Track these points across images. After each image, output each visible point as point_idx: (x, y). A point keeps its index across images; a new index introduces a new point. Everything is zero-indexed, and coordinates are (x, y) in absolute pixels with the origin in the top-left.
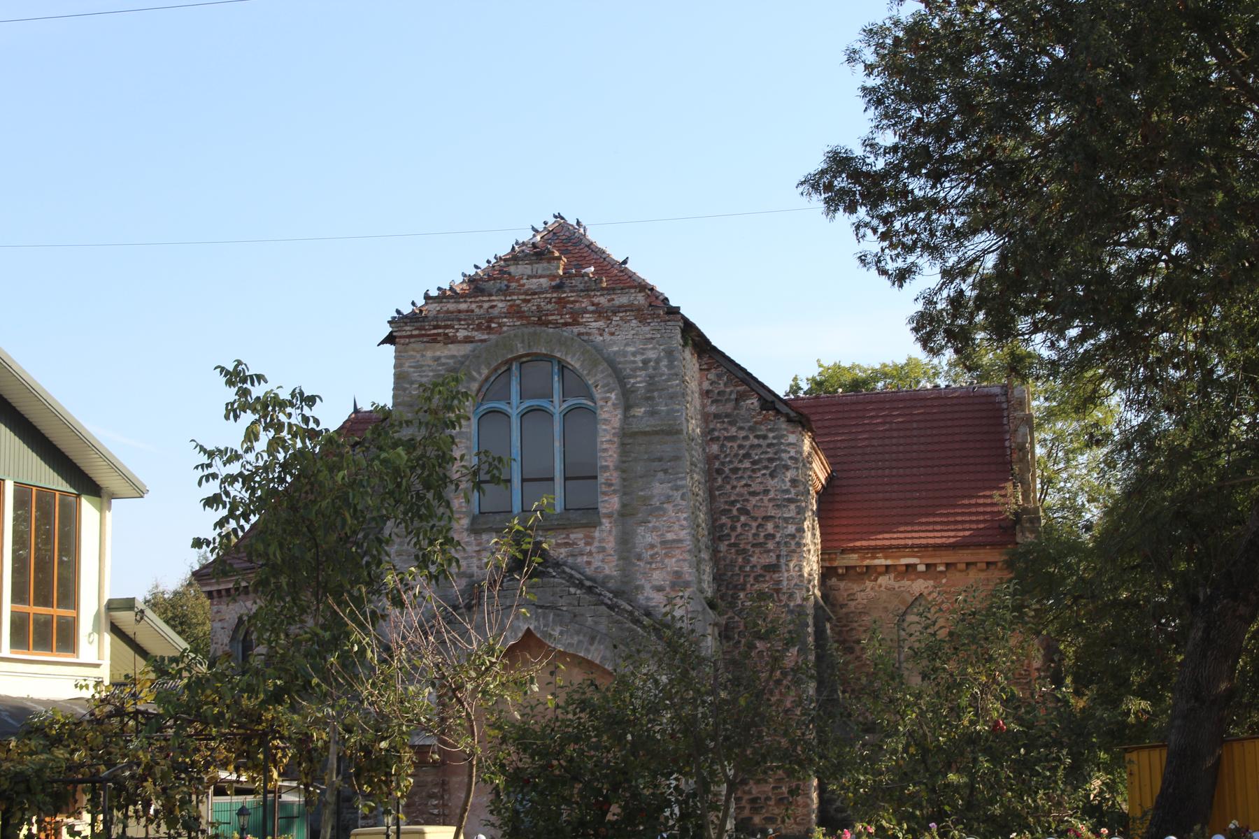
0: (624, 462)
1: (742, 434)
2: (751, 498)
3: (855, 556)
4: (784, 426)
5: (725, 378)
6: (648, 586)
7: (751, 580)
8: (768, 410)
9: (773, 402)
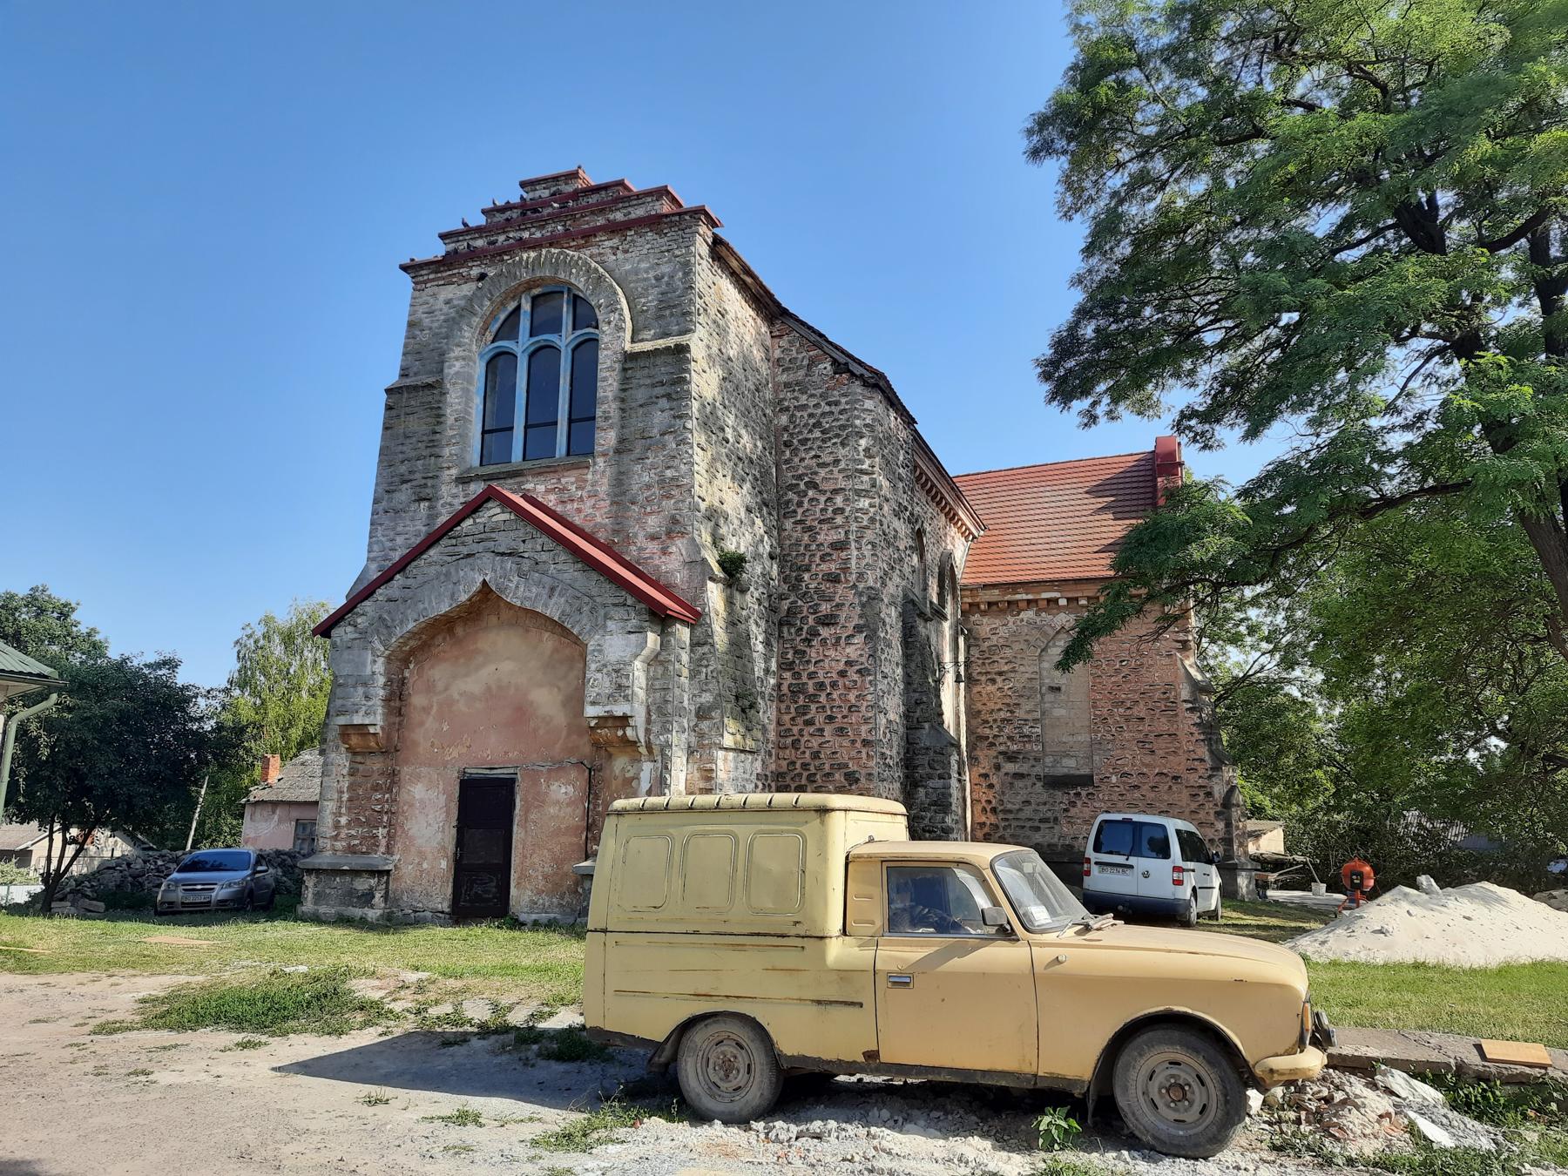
0: (624, 390)
1: (813, 402)
2: (820, 470)
3: (997, 592)
6: (641, 535)
7: (817, 560)
8: (841, 373)
9: (846, 364)
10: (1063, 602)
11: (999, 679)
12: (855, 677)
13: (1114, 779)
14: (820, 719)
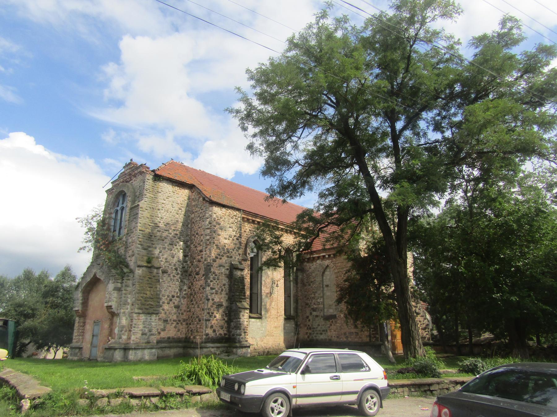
10: (327, 256)
11: (311, 284)
12: (202, 290)
14: (195, 303)
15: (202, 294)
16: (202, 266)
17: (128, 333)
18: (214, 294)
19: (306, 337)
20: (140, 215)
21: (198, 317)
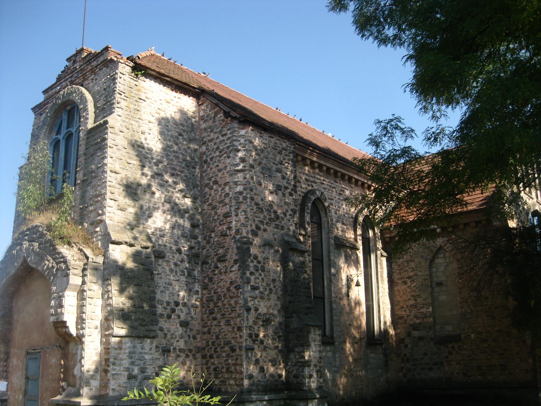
1: (216, 135)
4: (236, 125)
5: (210, 106)
7: (217, 224)
9: (229, 112)
11: (408, 281)
12: (234, 290)
13: (473, 336)
14: (219, 316)
15: (235, 299)
16: (229, 242)
17: (101, 376)
18: (258, 299)
19: (401, 374)
20: (110, 142)
21: (228, 343)
